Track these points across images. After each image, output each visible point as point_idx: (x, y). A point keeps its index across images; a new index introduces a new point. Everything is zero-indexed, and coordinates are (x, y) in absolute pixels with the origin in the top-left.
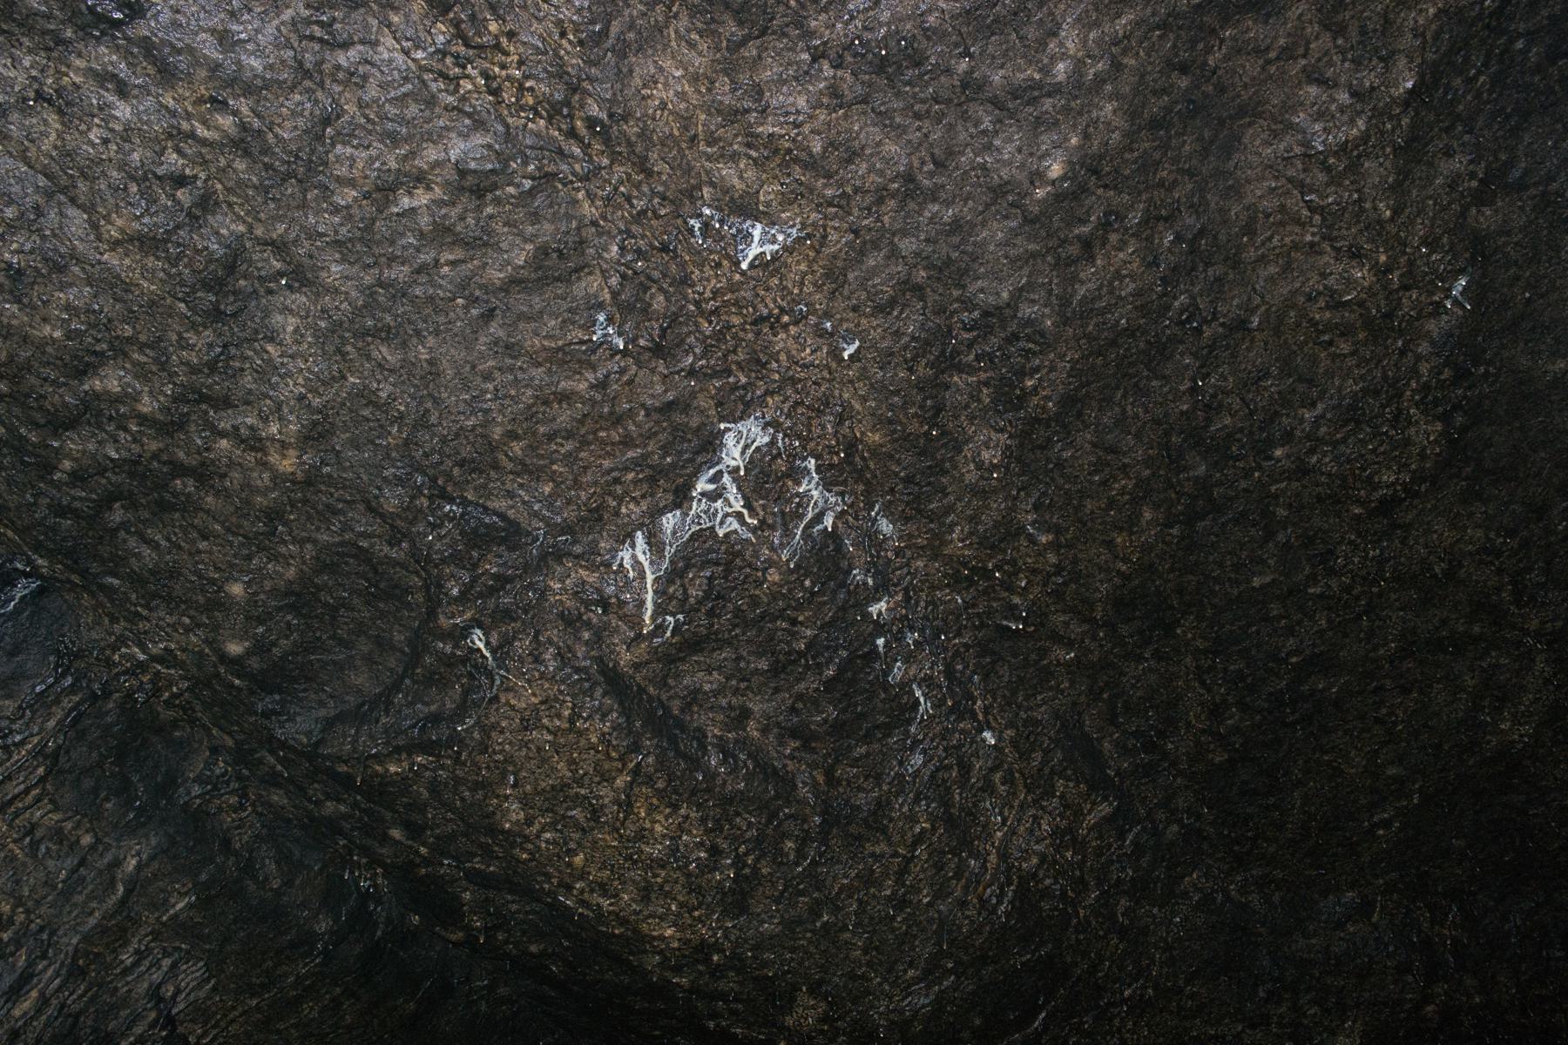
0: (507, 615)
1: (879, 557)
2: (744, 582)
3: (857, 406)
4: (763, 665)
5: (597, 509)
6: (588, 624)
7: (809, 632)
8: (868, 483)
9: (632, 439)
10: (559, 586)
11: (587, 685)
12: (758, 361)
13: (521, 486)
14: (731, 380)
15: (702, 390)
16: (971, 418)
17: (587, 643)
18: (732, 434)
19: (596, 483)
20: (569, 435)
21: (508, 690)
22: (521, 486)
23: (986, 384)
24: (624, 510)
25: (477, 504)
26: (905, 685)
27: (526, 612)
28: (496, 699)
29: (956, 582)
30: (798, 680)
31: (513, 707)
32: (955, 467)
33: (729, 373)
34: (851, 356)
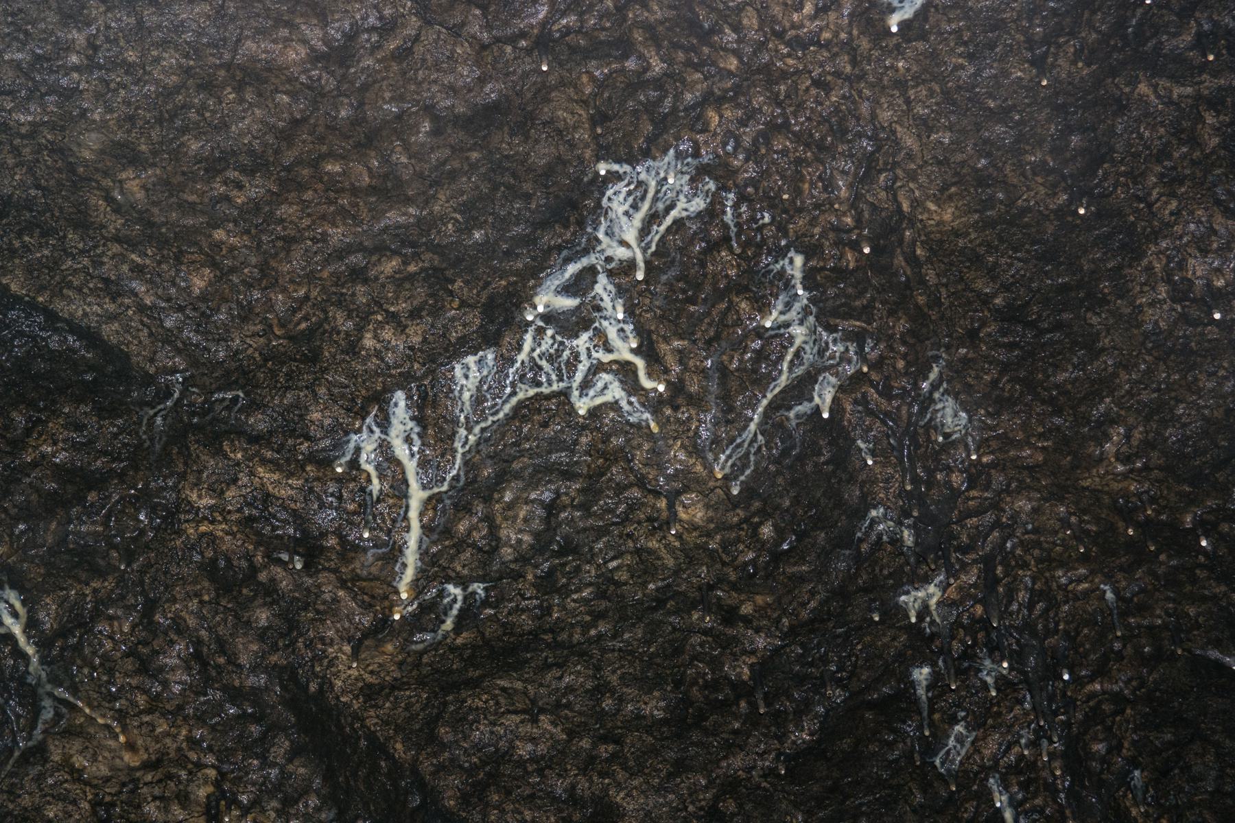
0: (86, 561)
1: (930, 483)
2: (626, 519)
3: (909, 141)
4: (654, 707)
5: (310, 333)
6: (270, 592)
7: (761, 642)
8: (919, 317)
9: (399, 184)
10: (214, 500)
11: (255, 730)
12: (693, 25)
13: (138, 270)
14: (631, 64)
15: (562, 83)
16: (1171, 182)
17: (262, 635)
18: (622, 188)
19: (311, 277)
20: (257, 165)
21: (70, 733)
22: (138, 270)
23: (1215, 103)
24: (369, 342)
25: (33, 306)
26: (971, 780)
27: (129, 557)
28: (39, 752)
29: (1105, 552)
30: (730, 748)
31: (76, 774)
32: (1122, 292)
33: (625, 47)
34: (903, 25)
